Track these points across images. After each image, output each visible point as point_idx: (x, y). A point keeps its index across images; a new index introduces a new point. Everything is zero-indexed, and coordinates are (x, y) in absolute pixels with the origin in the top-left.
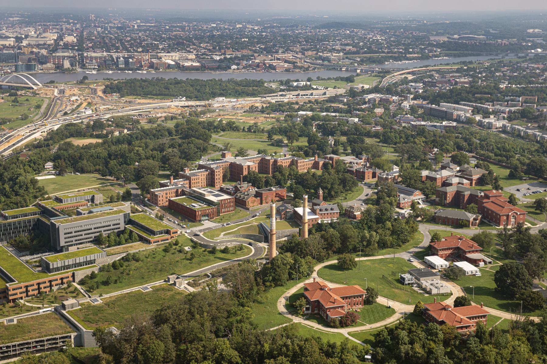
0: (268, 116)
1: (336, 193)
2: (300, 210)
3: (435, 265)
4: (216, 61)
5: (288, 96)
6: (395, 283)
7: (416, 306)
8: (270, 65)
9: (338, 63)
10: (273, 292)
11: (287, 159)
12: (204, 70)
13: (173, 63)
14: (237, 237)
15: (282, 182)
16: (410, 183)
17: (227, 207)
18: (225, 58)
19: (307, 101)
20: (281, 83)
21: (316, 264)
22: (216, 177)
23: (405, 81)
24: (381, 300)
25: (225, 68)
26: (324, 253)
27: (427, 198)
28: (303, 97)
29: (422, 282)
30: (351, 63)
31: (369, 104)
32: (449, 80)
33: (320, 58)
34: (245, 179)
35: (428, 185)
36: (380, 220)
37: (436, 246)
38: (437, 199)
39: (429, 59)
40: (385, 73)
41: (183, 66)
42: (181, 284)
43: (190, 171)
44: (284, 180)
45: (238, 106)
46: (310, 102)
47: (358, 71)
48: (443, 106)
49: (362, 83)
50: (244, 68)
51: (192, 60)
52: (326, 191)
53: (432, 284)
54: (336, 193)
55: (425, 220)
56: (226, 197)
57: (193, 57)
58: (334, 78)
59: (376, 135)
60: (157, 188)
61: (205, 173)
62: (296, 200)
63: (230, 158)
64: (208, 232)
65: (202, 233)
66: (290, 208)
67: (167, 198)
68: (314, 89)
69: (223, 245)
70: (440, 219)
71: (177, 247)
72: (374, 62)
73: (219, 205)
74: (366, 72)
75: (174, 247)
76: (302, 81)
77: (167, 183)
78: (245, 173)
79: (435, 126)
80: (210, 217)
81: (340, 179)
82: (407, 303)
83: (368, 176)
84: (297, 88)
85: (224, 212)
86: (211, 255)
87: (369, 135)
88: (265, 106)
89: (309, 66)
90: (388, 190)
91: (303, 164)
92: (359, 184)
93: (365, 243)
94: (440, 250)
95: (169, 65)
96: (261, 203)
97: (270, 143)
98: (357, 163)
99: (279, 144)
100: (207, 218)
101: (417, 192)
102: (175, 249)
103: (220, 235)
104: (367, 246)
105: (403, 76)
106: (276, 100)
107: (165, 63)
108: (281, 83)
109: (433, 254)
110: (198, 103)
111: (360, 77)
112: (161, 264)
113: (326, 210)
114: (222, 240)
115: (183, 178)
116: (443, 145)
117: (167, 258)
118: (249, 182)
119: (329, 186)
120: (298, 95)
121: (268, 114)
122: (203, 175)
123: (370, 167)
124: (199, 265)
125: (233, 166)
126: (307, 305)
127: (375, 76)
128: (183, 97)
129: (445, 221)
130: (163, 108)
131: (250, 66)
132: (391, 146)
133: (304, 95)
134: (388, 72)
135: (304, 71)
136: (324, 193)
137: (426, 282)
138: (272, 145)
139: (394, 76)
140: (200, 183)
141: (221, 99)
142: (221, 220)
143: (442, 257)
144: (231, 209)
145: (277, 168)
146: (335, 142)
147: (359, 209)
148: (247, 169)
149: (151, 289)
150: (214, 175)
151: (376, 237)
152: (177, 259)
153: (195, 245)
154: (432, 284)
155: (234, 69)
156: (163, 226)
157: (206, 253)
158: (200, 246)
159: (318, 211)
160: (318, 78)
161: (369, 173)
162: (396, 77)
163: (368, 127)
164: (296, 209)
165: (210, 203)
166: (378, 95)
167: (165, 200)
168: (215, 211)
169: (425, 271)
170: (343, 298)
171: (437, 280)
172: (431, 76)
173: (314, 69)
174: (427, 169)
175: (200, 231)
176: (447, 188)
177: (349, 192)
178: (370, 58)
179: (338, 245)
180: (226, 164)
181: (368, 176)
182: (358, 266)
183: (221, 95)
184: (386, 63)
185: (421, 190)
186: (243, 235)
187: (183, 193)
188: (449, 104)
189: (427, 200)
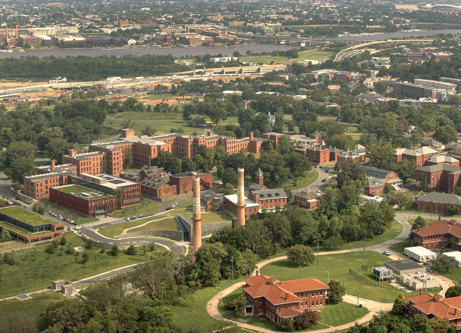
0: (182, 97)
1: (282, 177)
2: (233, 198)
3: (419, 257)
4: (107, 34)
5: (208, 74)
6: (368, 278)
7: (396, 301)
8: (181, 39)
9: (274, 35)
10: (200, 294)
11: (211, 139)
12: (91, 47)
13: (49, 38)
14: (146, 235)
15: (206, 166)
16: (380, 163)
18: (120, 31)
19: (234, 80)
20: (198, 59)
21: (259, 260)
22: (114, 162)
23: (367, 55)
24: (348, 299)
25: (120, 42)
26: (268, 246)
27: (405, 182)
28: (228, 74)
29: (403, 275)
30: (293, 35)
31: (319, 82)
32: (424, 55)
33: (250, 29)
34: (155, 162)
35: (406, 165)
36: (342, 207)
37: (419, 233)
38: (418, 183)
39: (396, 31)
40: (337, 47)
41: (62, 42)
42: (70, 291)
43: (78, 153)
44: (209, 164)
45: (140, 87)
46: (238, 80)
47: (303, 45)
48: (418, 83)
49: (309, 58)
50: (146, 42)
51: (73, 34)
52: (268, 175)
53: (415, 278)
54: (282, 177)
55: (403, 208)
56: (128, 183)
57: (77, 31)
58: (270, 53)
59: (333, 112)
60: (34, 175)
61: (99, 156)
62: (229, 182)
63: (131, 137)
64: (105, 228)
65: (98, 230)
66: (218, 197)
67: (47, 187)
68: (243, 65)
69: (128, 245)
70: (422, 205)
71: (64, 247)
72: (323, 34)
73: (119, 193)
74: (314, 46)
75: (60, 247)
76: (226, 56)
77: (47, 169)
78: (154, 155)
79: (410, 103)
80: (108, 210)
81: (286, 160)
82: (384, 301)
83: (325, 158)
84: (218, 65)
86: (111, 257)
87: (322, 111)
88: (176, 86)
89: (235, 39)
90: (353, 172)
91: (234, 145)
92: (313, 167)
93: (324, 233)
94: (425, 238)
95: (43, 41)
96: (178, 193)
97: (187, 124)
98: (308, 143)
99: (199, 124)
100: (103, 211)
101: (392, 174)
102: (62, 249)
103: (122, 232)
104: (328, 236)
105: (363, 50)
107: (38, 39)
108: (198, 59)
109: (416, 245)
110: (83, 84)
111: (306, 51)
112: (43, 268)
114: (125, 238)
115: (68, 163)
116: (421, 121)
117: (50, 261)
118: (159, 166)
119: (272, 168)
120: (222, 72)
121: (180, 95)
122: (96, 159)
123: (327, 146)
124: (95, 270)
125: (136, 146)
126: (248, 304)
127: (326, 50)
128: (63, 77)
129: (430, 208)
130: (36, 91)
131: (154, 40)
132: (352, 124)
133: (230, 73)
134: (342, 45)
135: (228, 45)
136: (265, 177)
137: (408, 276)
138: (190, 126)
139: (351, 50)
140: (92, 169)
142: (123, 213)
143: (427, 248)
144: (137, 199)
145: (199, 149)
146: (276, 120)
147: (313, 195)
148: (156, 151)
149: (31, 298)
150: (111, 158)
151: (339, 223)
152: (64, 262)
153: (89, 245)
154: (415, 278)
155: (132, 45)
156: (44, 221)
157: (104, 254)
158: (95, 246)
159: (258, 197)
160: (249, 53)
161: (324, 156)
162: (355, 50)
163: (321, 104)
164: (228, 197)
165: (107, 191)
166: (332, 70)
167: (44, 190)
168: (115, 202)
169: (406, 262)
170: (297, 294)
171: (422, 273)
172: (400, 50)
173: (243, 42)
174: (403, 147)
175: (95, 227)
176: (431, 167)
177: (300, 178)
178: (318, 29)
179: (287, 236)
180: (127, 144)
181: (325, 158)
182: (315, 262)
184: (340, 36)
185: (396, 171)
186: (154, 232)
187: (70, 180)
188: (426, 80)
189: (405, 184)
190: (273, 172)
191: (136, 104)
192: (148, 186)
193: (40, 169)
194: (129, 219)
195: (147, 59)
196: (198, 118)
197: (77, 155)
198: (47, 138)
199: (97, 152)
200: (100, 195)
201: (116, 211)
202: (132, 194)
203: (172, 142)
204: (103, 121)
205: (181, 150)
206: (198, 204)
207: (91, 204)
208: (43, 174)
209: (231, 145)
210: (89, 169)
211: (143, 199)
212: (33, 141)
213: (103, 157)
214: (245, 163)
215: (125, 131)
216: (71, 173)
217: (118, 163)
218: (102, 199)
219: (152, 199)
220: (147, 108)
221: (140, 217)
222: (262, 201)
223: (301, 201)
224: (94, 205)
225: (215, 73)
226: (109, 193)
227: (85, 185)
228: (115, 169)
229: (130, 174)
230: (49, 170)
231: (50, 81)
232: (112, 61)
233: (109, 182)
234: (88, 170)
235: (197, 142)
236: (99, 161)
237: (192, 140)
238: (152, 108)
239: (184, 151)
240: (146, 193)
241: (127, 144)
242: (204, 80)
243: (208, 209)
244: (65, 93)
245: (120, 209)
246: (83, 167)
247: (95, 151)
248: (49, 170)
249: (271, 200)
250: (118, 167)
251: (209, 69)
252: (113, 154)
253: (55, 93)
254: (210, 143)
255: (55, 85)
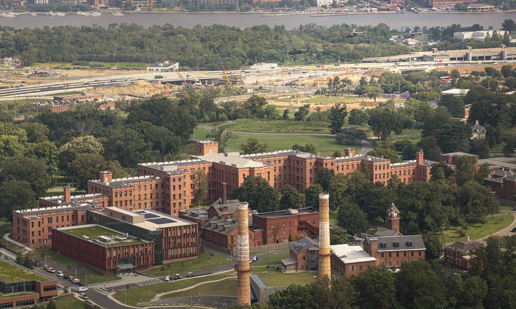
17: (180, 246)
22: (172, 192)
45: (306, 81)
61: (148, 183)
63: (211, 155)
77: (56, 200)
80: (139, 265)
84: (462, 45)
85: (173, 257)
100: (130, 266)
106: (404, 68)
113: (396, 245)
119: (420, 204)
120: (466, 58)
133: (481, 58)
141: (265, 67)
144: (192, 250)
150: (168, 187)
159: (374, 247)
165: (141, 233)
183: (271, 59)
187: (89, 217)
190: (422, 211)
191: (264, 107)
192: (216, 231)
193: (45, 201)
194: (168, 279)
195: (337, 33)
196: (353, 129)
197: (114, 180)
198: (73, 154)
199: (147, 177)
200: (129, 241)
201: (154, 267)
202: (184, 241)
203: (282, 164)
204: (192, 132)
205: (296, 178)
206: (245, 246)
207: (111, 254)
208: (46, 207)
209: (381, 172)
210: (129, 203)
211: (202, 251)
212: (50, 158)
213: (157, 185)
214: (386, 197)
215: (203, 144)
216: (93, 207)
217: (180, 195)
218: (128, 247)
219: (219, 250)
220: (281, 114)
221: (188, 277)
222: (383, 254)
223: (454, 258)
224: (115, 255)
225: (452, 59)
226: (144, 239)
227: (111, 227)
228: (175, 204)
229: (194, 212)
230: (60, 202)
231: (148, 68)
232: (274, 36)
233: (147, 220)
234: (126, 204)
235: (322, 164)
236: (149, 191)
237: (313, 161)
238: (291, 116)
239: (300, 179)
240: (213, 242)
241: (202, 166)
242: (427, 71)
243: (299, 266)
245: (161, 264)
246: (119, 199)
247: (145, 174)
248: (60, 202)
249: (398, 253)
250: (180, 201)
251: (442, 52)
252: (172, 180)
253: (153, 89)
254: (340, 168)
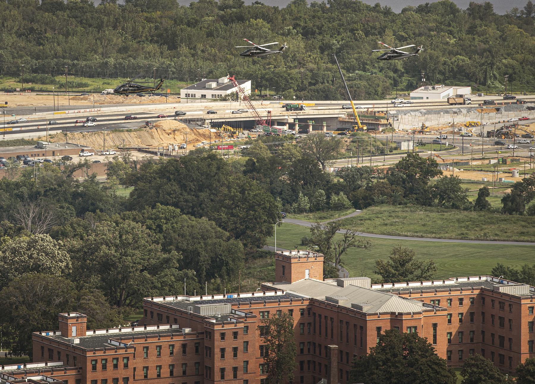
61: (165, 341)
128: (239, 77)
150: (210, 350)
191: (434, 180)
203: (465, 309)
205: (497, 341)
213: (184, 346)
215: (289, 258)
231: (183, 92)
238: (495, 202)
241: (285, 306)
244: (228, 141)
252: (217, 336)
255: (195, 109)
